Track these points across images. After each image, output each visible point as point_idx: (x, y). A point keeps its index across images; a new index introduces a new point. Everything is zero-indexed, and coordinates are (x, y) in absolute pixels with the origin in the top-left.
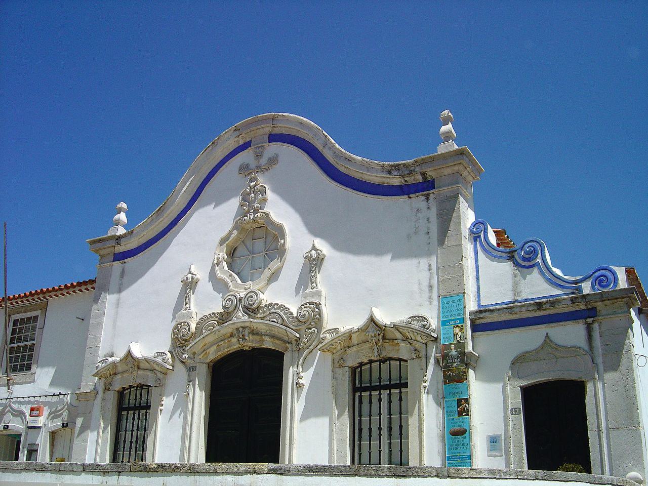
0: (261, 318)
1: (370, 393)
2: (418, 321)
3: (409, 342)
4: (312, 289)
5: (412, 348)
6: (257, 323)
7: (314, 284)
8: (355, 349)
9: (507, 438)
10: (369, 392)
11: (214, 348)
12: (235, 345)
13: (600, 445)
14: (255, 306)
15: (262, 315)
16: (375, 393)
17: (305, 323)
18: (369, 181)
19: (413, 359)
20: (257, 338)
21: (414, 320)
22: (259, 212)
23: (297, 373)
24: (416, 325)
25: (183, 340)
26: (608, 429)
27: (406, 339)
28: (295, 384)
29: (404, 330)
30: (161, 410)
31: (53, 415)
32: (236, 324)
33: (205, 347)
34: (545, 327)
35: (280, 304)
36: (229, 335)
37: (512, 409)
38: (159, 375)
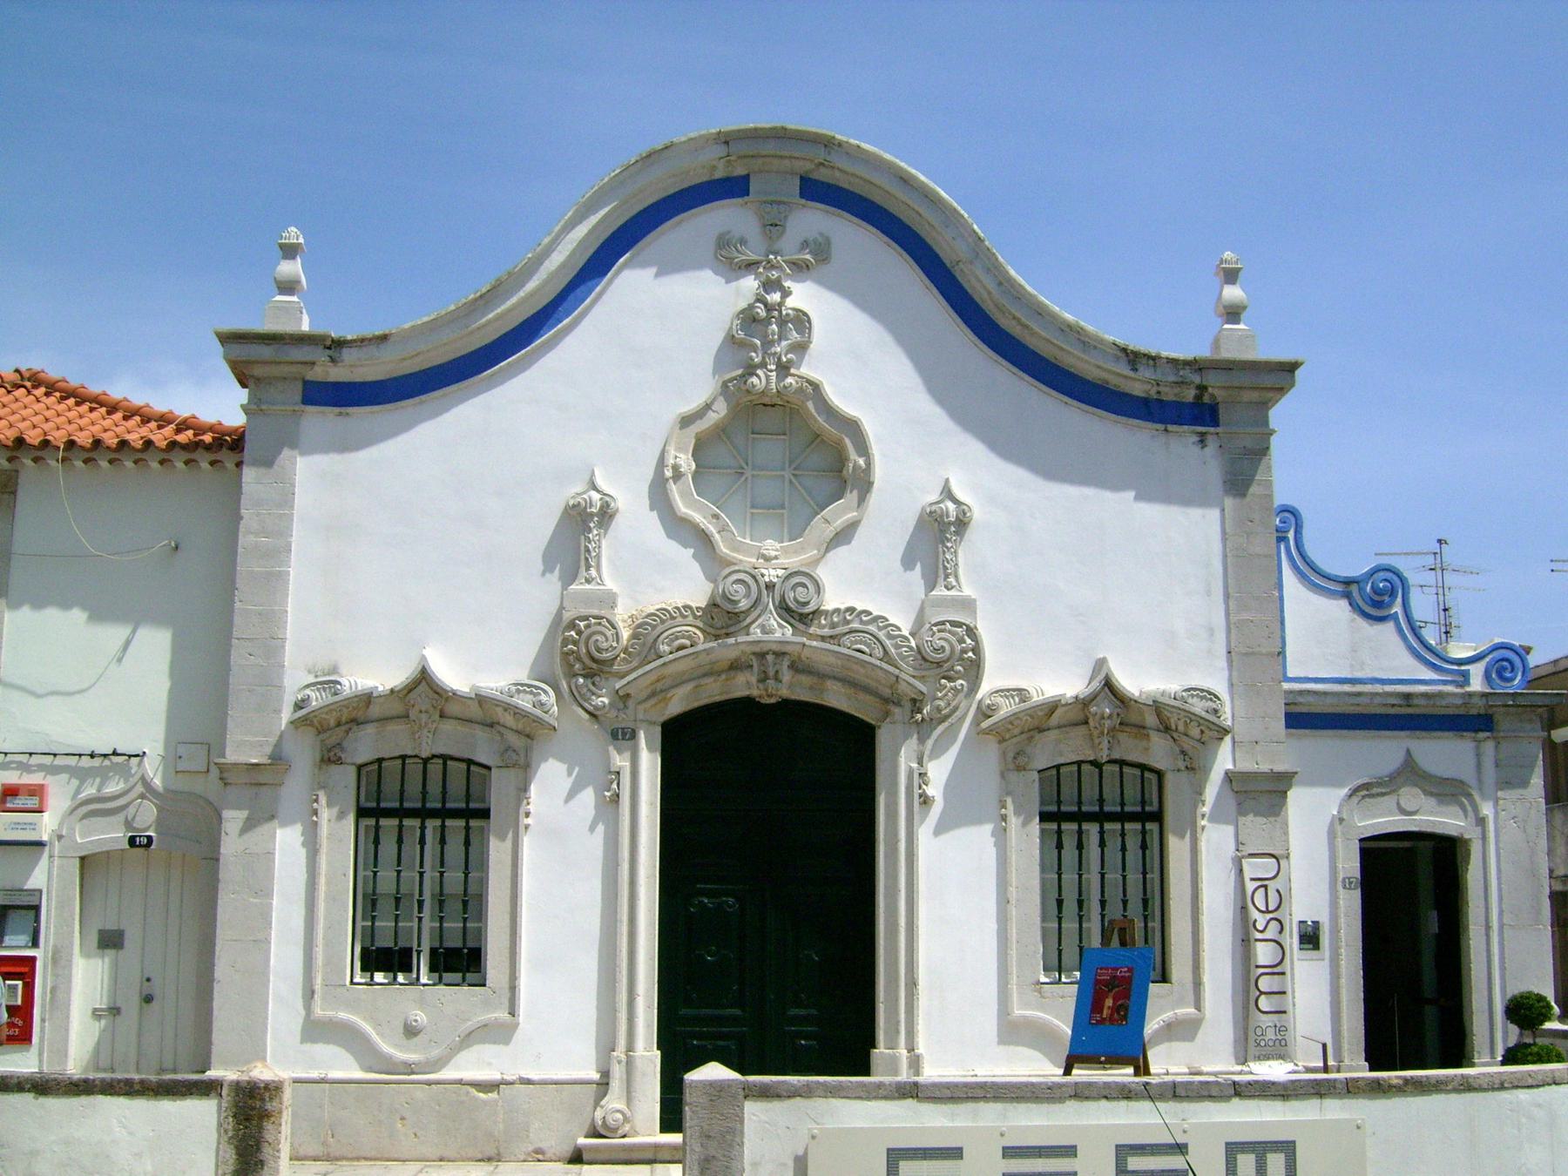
0: (823, 638)
1: (443, 822)
2: (1202, 698)
3: (1172, 737)
4: (946, 587)
5: (1177, 750)
6: (811, 643)
7: (952, 580)
8: (1053, 734)
9: (1335, 930)
10: (464, 820)
11: (689, 687)
12: (743, 686)
13: (1488, 951)
14: (807, 610)
15: (826, 632)
16: (432, 824)
17: (939, 664)
18: (1072, 370)
19: (1178, 770)
20: (805, 680)
21: (1193, 696)
22: (793, 375)
23: (920, 774)
24: (1198, 707)
25: (593, 659)
26: (1501, 926)
27: (1166, 729)
28: (916, 796)
29: (1171, 712)
30: (527, 827)
31: (92, 809)
32: (761, 645)
33: (659, 686)
34: (1407, 737)
35: (875, 613)
36: (725, 665)
37: (1344, 879)
38: (513, 739)
